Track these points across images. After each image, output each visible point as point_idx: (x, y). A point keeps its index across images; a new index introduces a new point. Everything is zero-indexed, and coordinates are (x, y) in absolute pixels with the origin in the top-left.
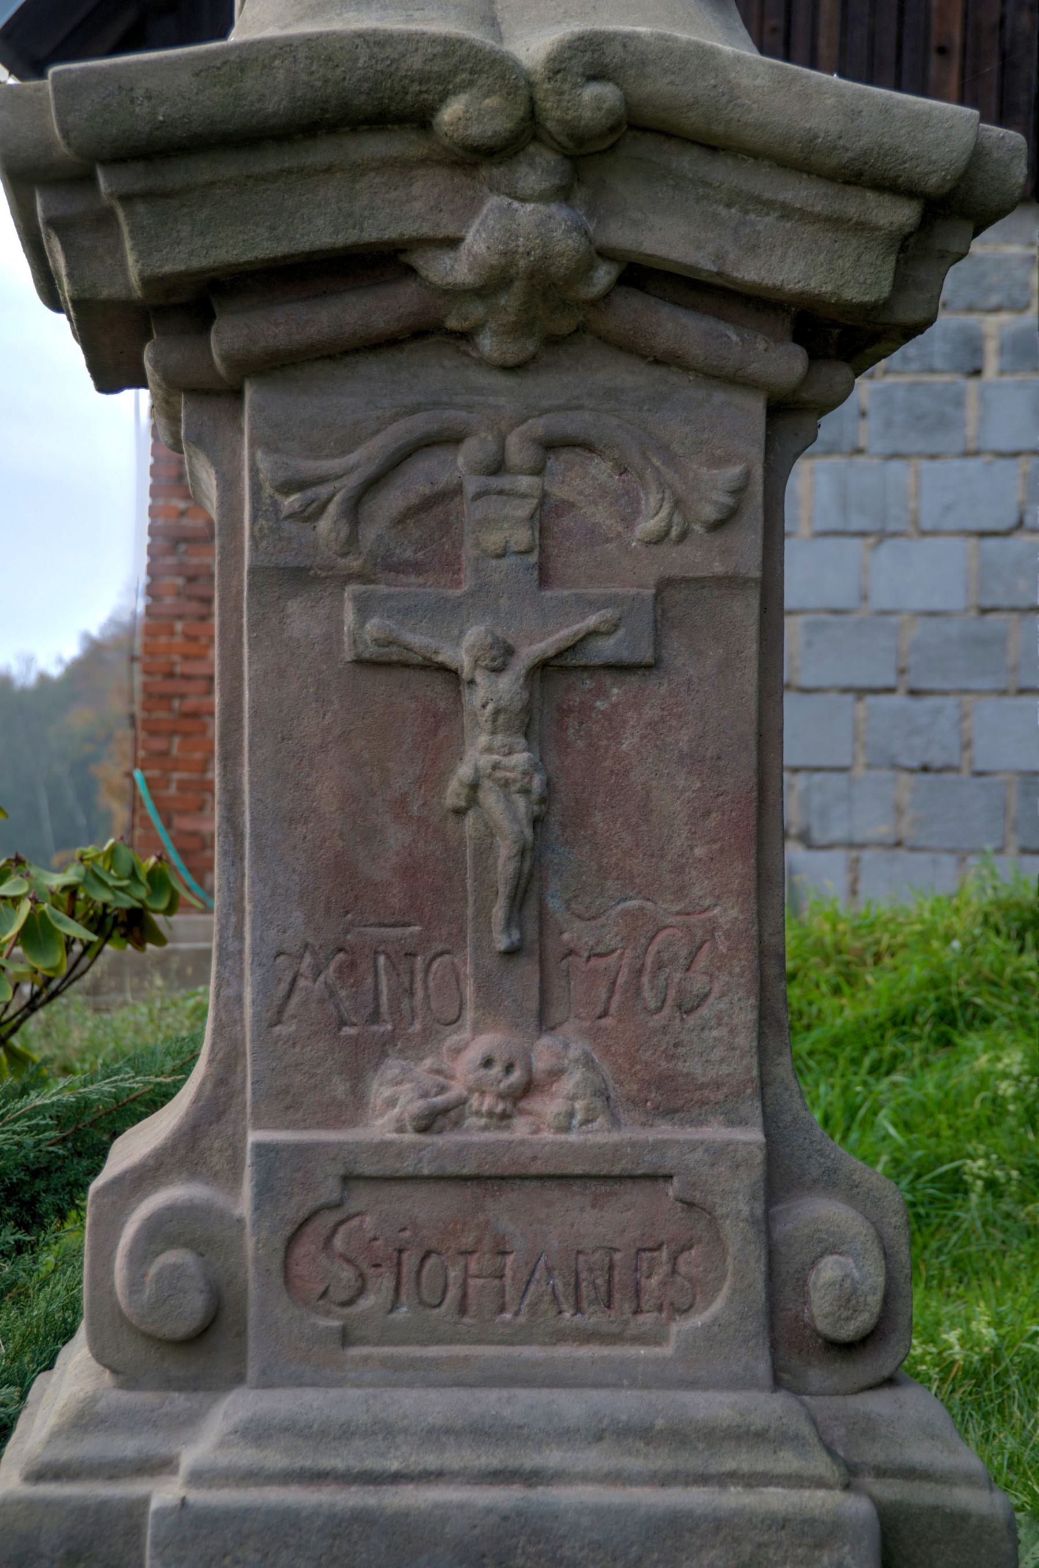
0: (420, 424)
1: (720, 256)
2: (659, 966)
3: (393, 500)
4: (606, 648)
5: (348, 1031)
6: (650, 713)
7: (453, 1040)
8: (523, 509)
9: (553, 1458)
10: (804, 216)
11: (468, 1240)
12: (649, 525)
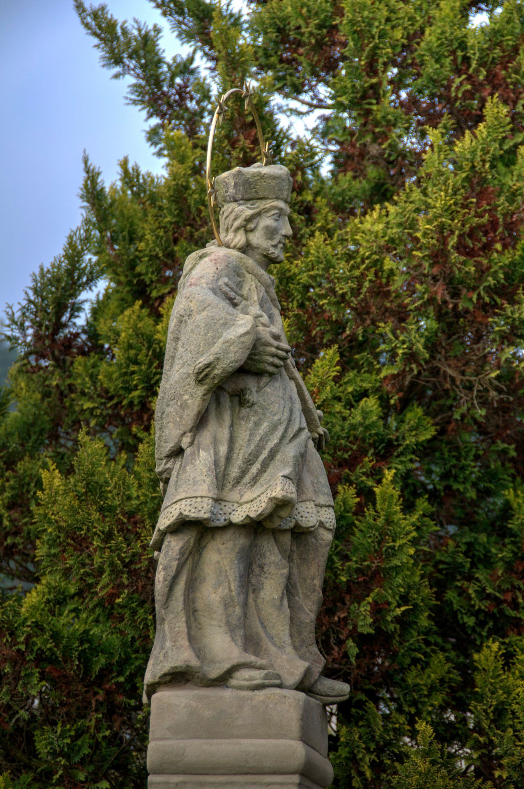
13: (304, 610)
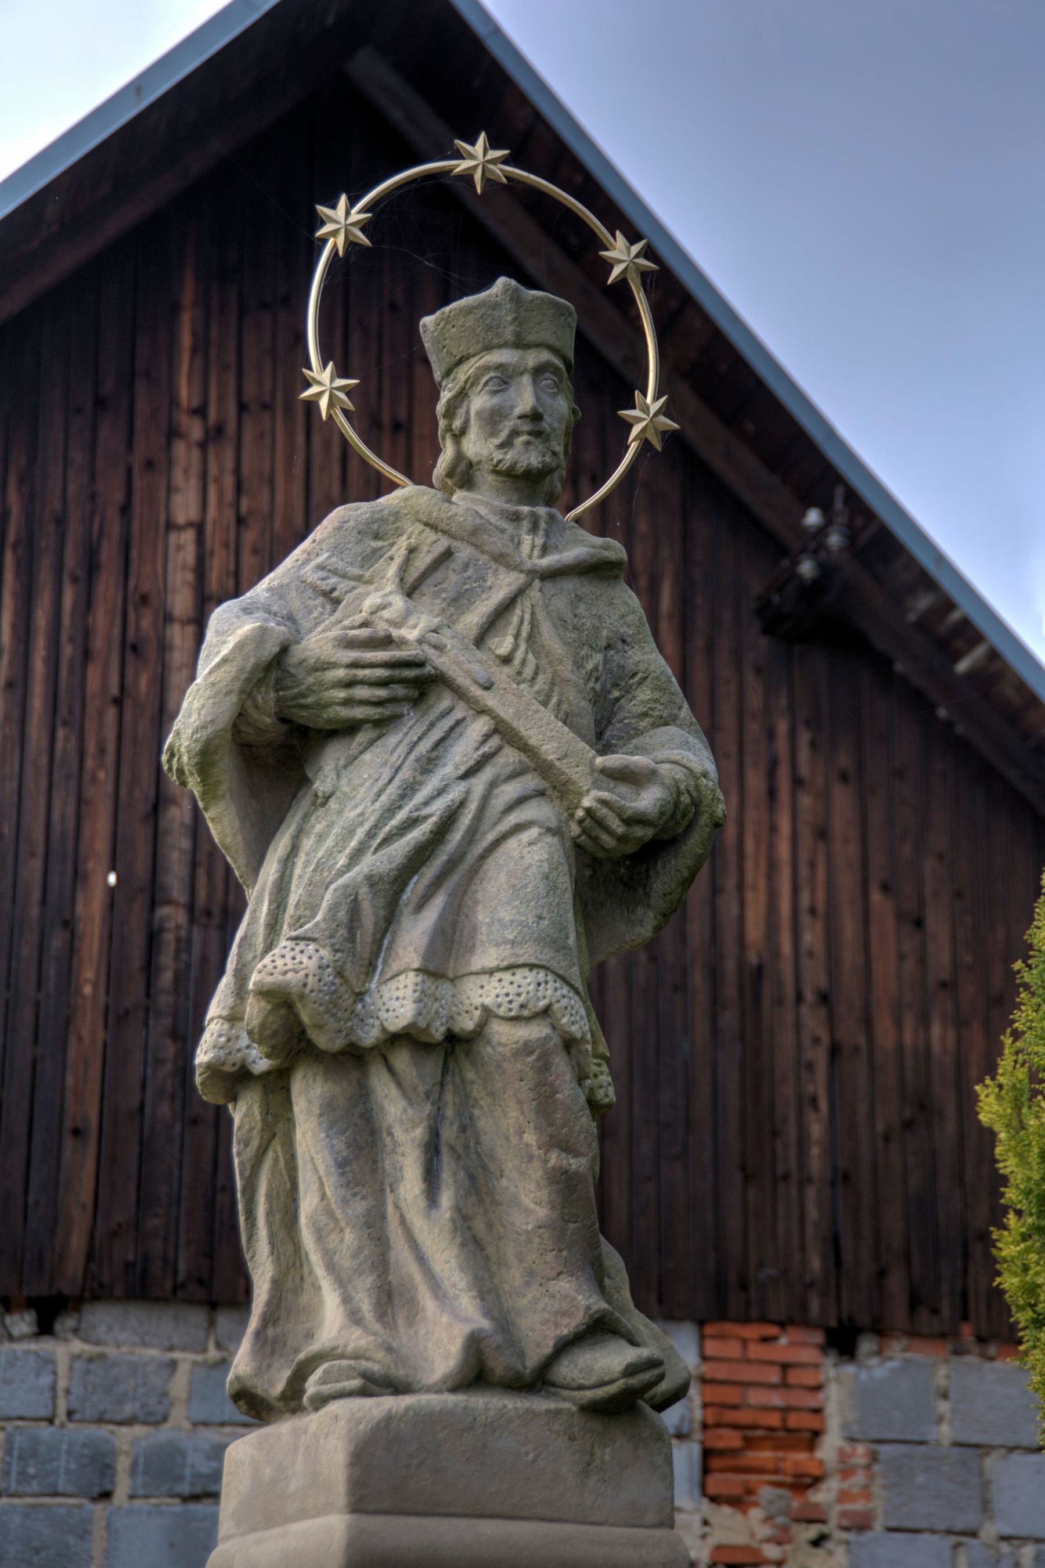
13: (519, 1205)
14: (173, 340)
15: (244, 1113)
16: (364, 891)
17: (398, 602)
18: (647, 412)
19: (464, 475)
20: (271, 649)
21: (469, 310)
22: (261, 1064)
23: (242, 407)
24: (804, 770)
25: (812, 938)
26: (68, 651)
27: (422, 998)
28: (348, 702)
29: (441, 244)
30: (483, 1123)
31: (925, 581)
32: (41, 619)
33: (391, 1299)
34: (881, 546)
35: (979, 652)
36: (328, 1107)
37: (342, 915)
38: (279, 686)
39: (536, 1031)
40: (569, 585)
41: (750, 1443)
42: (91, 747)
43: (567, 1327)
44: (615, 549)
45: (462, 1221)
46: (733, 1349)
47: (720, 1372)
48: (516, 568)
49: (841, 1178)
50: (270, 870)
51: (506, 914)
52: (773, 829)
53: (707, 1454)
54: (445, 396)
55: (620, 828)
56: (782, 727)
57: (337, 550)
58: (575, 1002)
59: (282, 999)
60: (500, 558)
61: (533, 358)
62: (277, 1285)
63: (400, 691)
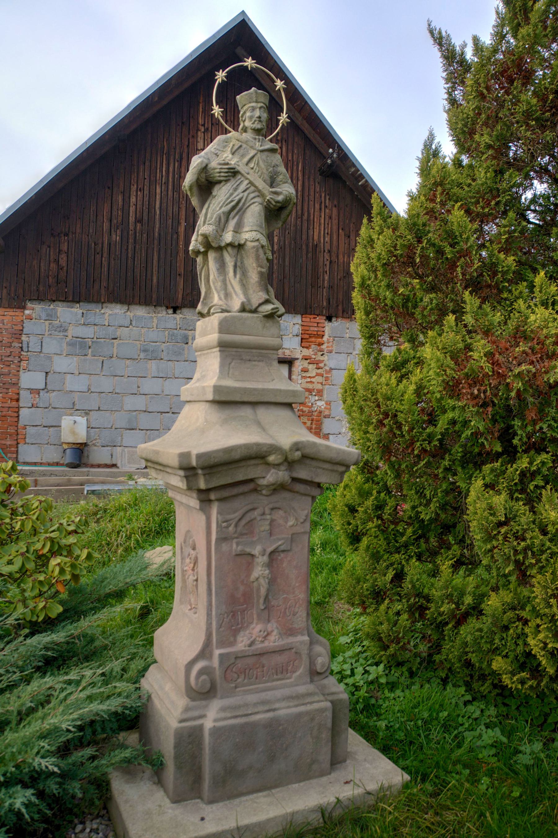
0: (250, 507)
1: (312, 477)
2: (290, 607)
3: (243, 522)
4: (282, 548)
5: (233, 628)
6: (289, 559)
7: (252, 626)
8: (268, 522)
9: (277, 705)
10: (327, 470)
11: (258, 666)
12: (290, 523)
14: (198, 110)
15: (199, 260)
16: (222, 215)
17: (230, 156)
18: (283, 118)
19: (245, 130)
20: (204, 165)
21: (246, 95)
22: (202, 250)
23: (212, 124)
24: (327, 204)
25: (327, 239)
26: (176, 176)
27: (233, 236)
28: (219, 176)
29: (242, 80)
30: (245, 262)
31: (354, 165)
32: (171, 169)
33: (227, 295)
34: (344, 157)
35: (364, 180)
36: (215, 258)
37: (217, 220)
38: (206, 173)
39: (256, 244)
40: (266, 153)
41: (310, 337)
42: (181, 196)
43: (261, 301)
44: (276, 146)
45: (241, 281)
46: (308, 320)
47: (305, 324)
48: (255, 149)
49: (331, 287)
50: (204, 211)
51: (250, 220)
52: (320, 216)
53: (302, 339)
54: (241, 113)
55: (274, 204)
56: (323, 195)
57: (218, 145)
58: (264, 238)
59: (205, 236)
60: (252, 147)
61: (260, 105)
62: (206, 293)
63: (230, 174)
